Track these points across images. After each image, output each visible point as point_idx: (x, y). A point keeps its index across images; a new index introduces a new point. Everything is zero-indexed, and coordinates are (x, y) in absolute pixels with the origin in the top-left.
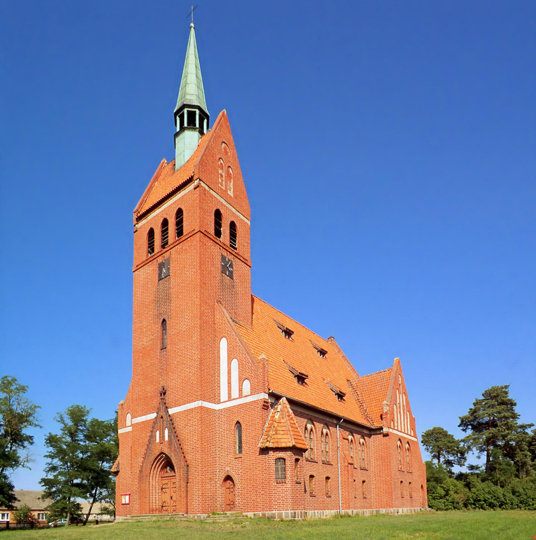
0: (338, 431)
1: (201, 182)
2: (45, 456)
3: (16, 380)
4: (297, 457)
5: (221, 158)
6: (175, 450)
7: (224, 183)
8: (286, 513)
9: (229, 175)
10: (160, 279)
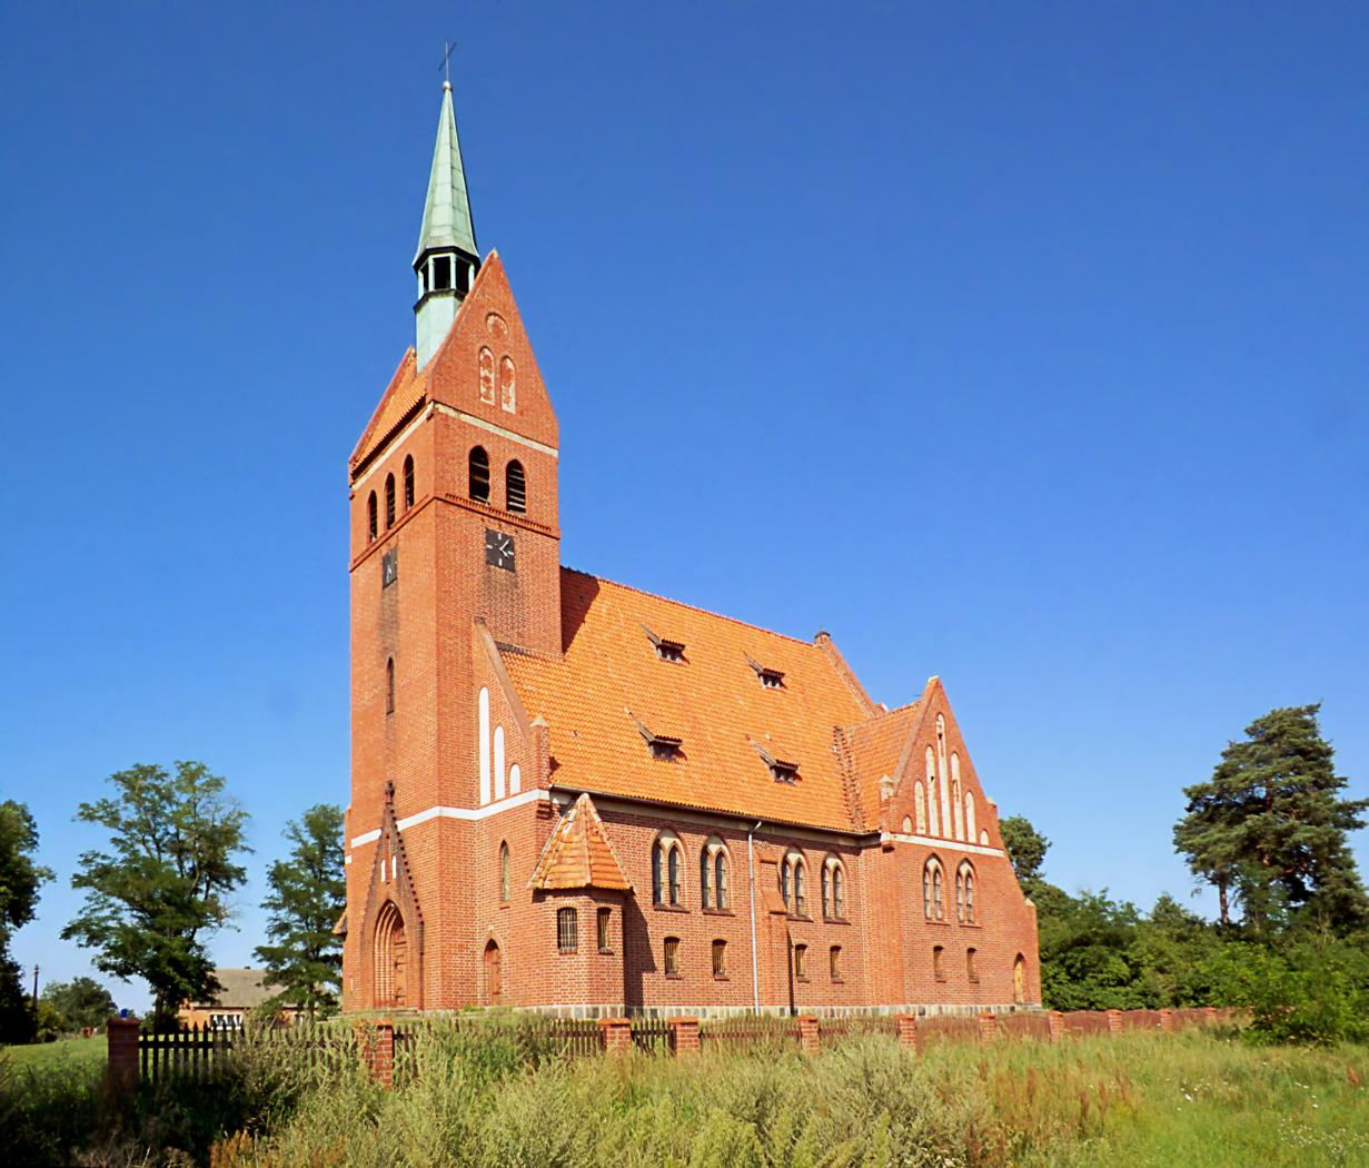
0: (750, 845)
1: (438, 406)
2: (262, 906)
3: (204, 768)
4: (603, 905)
5: (486, 347)
6: (405, 896)
7: (492, 393)
8: (577, 1009)
9: (504, 375)
10: (385, 586)
